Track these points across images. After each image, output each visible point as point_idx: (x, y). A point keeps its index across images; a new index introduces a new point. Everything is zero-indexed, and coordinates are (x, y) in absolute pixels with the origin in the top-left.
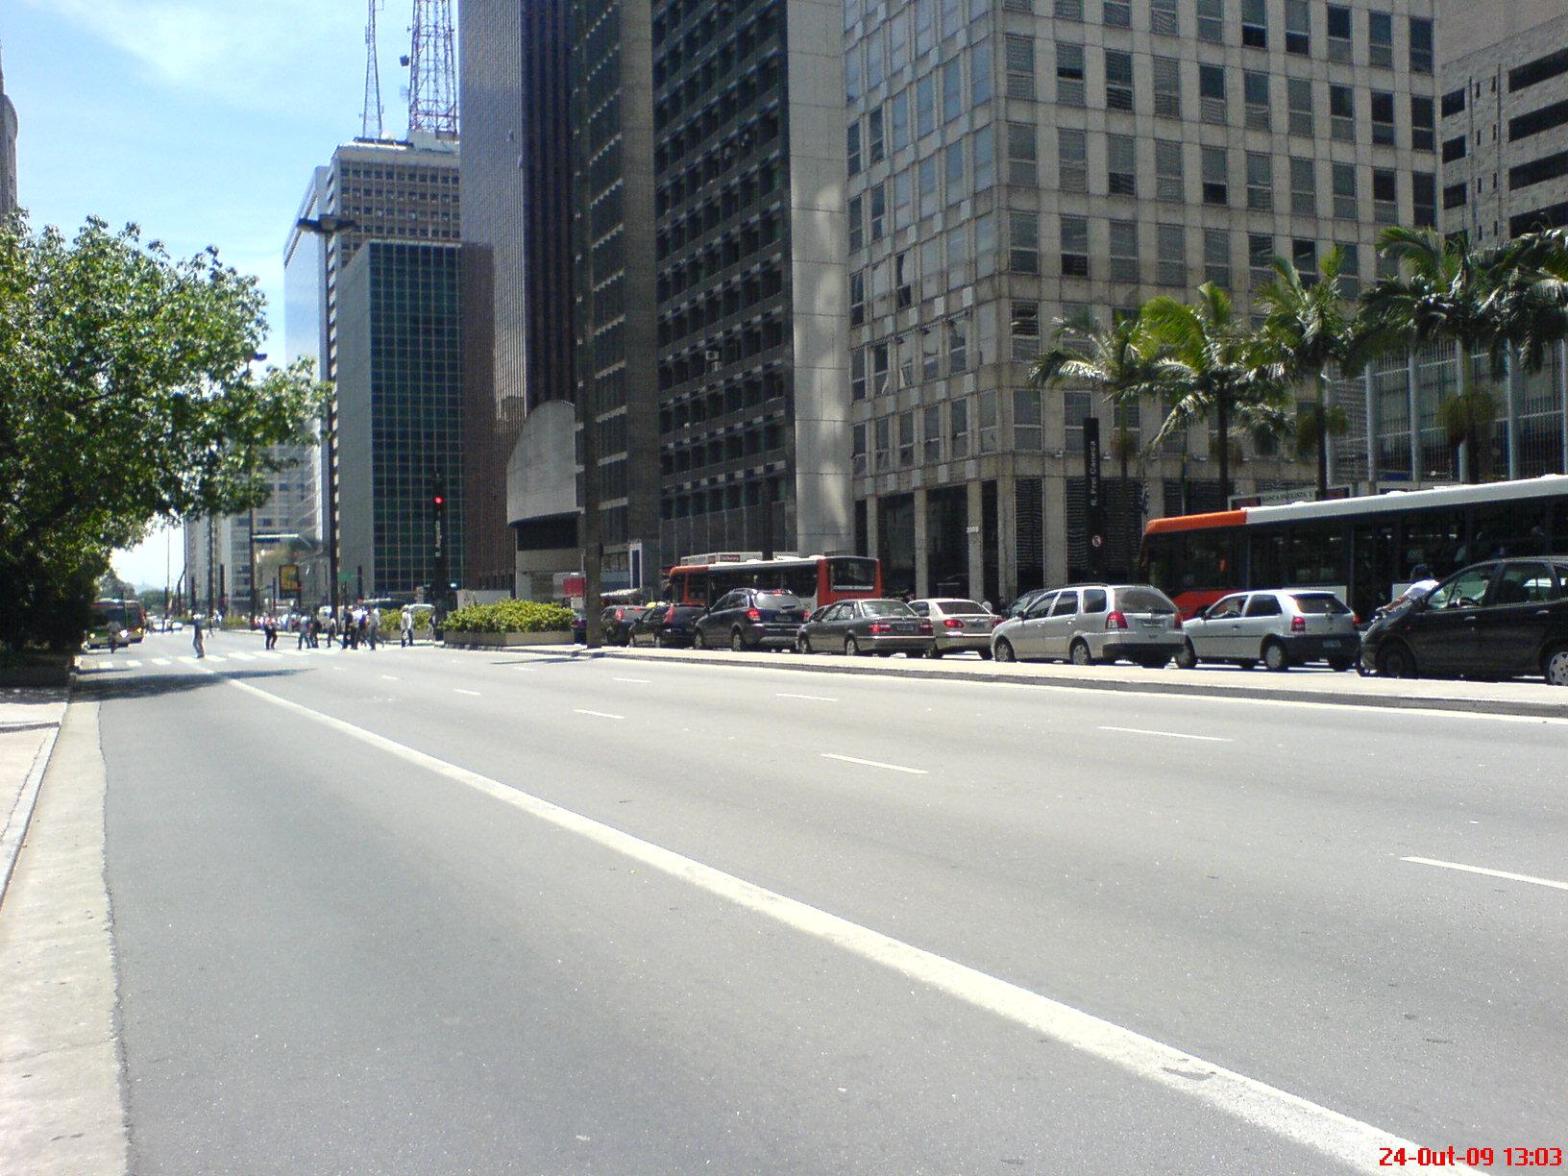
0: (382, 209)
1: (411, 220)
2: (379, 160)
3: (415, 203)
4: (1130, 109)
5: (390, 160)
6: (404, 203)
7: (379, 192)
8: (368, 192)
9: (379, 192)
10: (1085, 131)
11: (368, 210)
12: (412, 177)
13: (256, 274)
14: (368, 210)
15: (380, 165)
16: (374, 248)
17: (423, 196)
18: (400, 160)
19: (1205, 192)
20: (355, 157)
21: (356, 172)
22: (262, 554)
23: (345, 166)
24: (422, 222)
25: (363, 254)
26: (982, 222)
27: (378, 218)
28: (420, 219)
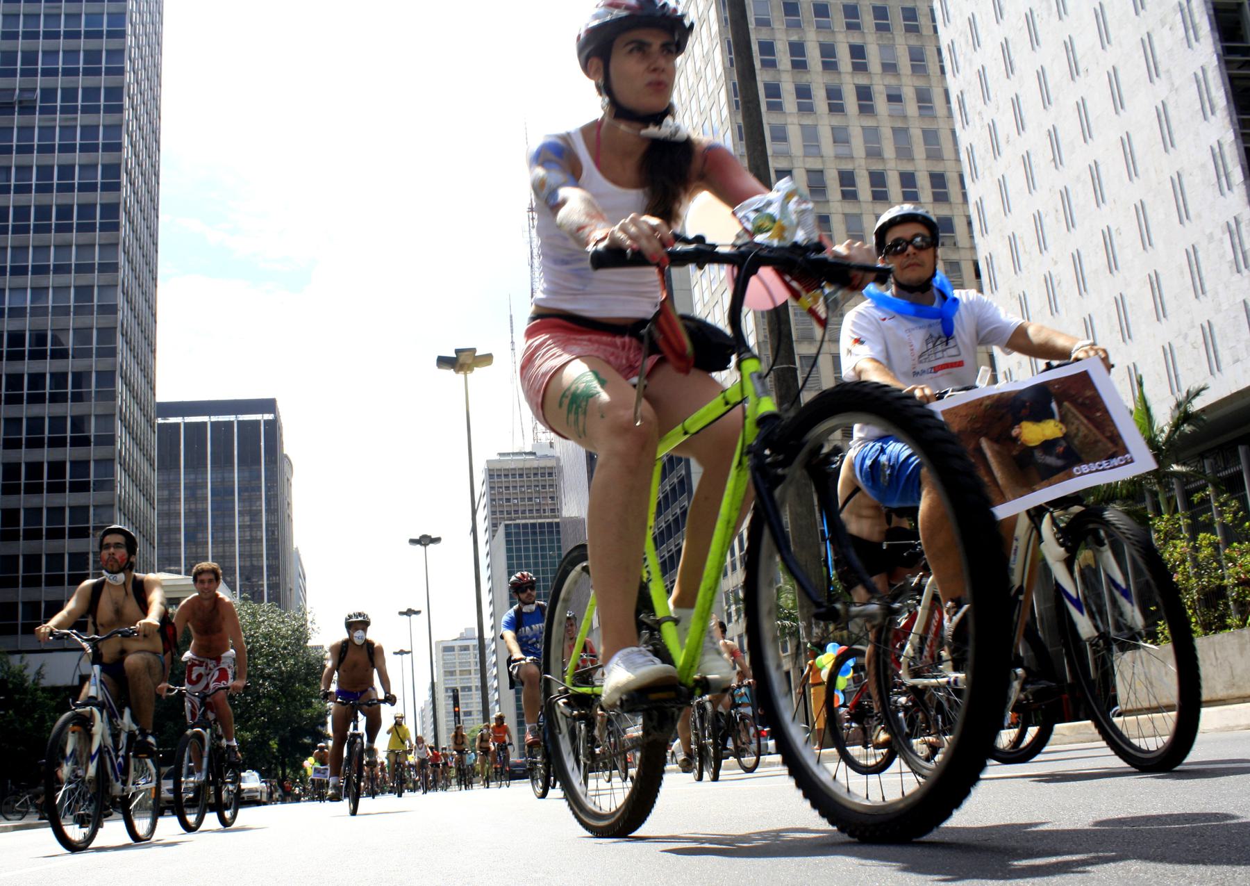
0: (517, 499)
1: (537, 504)
2: (513, 467)
3: (539, 492)
4: (848, 142)
5: (521, 466)
6: (531, 493)
7: (515, 487)
8: (507, 488)
9: (515, 487)
10: (861, 214)
11: (508, 500)
12: (535, 474)
13: (408, 544)
14: (508, 500)
15: (515, 469)
16: (507, 526)
17: (544, 487)
18: (528, 465)
19: (773, 110)
20: (498, 466)
21: (499, 476)
22: (258, 794)
23: (492, 473)
24: (544, 504)
25: (501, 530)
26: (739, 398)
27: (514, 505)
28: (542, 502)
